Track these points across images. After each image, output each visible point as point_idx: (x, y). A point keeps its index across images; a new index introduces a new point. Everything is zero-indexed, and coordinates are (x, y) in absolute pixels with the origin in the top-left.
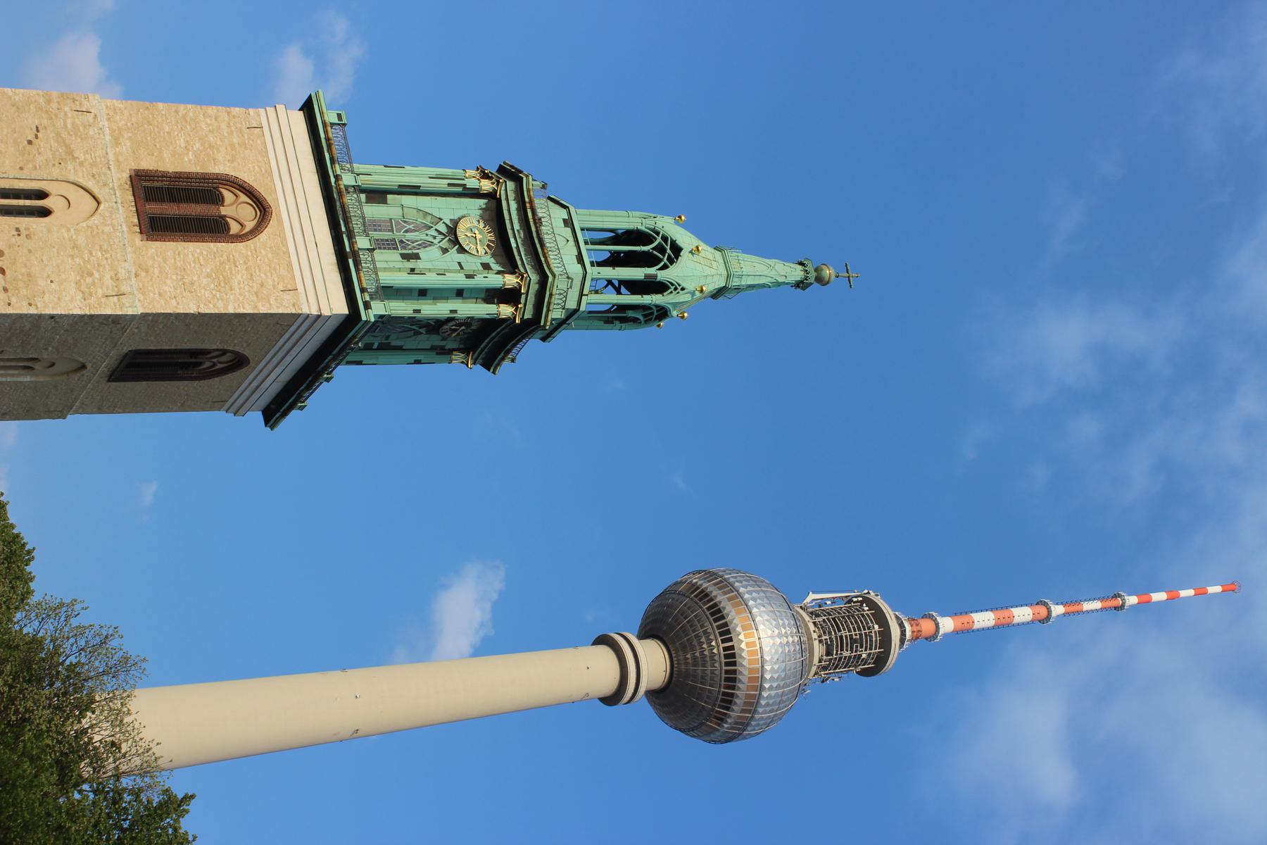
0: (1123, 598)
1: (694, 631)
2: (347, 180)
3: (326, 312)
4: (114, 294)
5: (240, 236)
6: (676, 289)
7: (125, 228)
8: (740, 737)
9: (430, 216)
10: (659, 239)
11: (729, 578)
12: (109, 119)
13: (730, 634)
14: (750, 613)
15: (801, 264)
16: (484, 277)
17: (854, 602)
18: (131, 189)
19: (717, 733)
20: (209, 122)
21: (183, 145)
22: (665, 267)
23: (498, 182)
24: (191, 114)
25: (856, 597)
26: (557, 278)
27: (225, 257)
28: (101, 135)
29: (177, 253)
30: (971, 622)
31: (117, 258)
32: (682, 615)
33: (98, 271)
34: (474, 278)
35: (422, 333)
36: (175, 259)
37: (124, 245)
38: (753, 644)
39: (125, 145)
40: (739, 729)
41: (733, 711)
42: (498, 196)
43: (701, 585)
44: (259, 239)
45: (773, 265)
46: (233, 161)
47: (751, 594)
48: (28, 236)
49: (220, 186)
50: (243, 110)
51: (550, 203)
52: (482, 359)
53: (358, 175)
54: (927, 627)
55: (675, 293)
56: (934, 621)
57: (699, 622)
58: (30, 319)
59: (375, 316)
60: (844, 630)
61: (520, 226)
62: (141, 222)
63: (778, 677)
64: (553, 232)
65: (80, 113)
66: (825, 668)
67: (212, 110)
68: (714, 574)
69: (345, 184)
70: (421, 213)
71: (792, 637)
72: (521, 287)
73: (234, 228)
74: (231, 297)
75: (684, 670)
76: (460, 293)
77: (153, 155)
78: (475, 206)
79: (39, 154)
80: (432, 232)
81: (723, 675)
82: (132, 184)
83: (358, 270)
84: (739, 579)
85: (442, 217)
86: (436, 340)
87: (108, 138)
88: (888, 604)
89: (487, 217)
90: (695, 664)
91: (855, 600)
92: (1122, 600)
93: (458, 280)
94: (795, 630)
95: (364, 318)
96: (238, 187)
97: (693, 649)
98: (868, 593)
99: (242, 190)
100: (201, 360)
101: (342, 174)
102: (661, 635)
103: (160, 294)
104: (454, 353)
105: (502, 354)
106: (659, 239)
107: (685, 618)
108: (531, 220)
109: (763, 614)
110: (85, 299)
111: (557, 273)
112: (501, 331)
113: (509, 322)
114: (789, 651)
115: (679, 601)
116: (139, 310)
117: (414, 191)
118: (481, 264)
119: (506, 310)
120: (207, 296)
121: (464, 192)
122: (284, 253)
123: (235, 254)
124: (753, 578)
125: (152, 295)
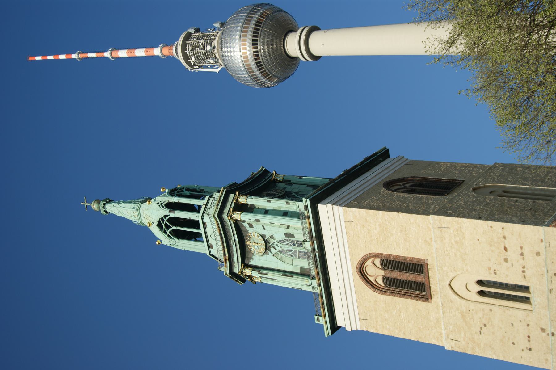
1: (271, 58)
2: (315, 282)
3: (329, 206)
4: (444, 229)
5: (374, 256)
6: (162, 204)
7: (436, 267)
8: (256, 5)
9: (279, 258)
10: (168, 232)
11: (253, 82)
12: (441, 334)
14: (243, 64)
15: (107, 212)
16: (250, 219)
17: (197, 66)
18: (431, 291)
19: (266, 8)
20: (387, 326)
22: (166, 216)
23: (242, 273)
24: (397, 331)
25: (196, 69)
26: (213, 214)
29: (409, 250)
30: (146, 52)
31: (441, 251)
32: (276, 67)
34: (256, 219)
35: (295, 193)
36: (410, 247)
37: (437, 258)
38: (243, 49)
40: (255, 9)
41: (257, 18)
42: (243, 265)
43: (266, 80)
45: (119, 213)
46: (376, 301)
47: (242, 73)
48: (490, 269)
49: (384, 288)
50: (369, 331)
51: (217, 256)
52: (267, 176)
53: (310, 285)
54: (166, 51)
55: (162, 202)
58: (493, 218)
59: (301, 201)
60: (202, 53)
61: (232, 247)
62: (427, 271)
64: (216, 241)
65: (457, 340)
66: (213, 35)
67: (385, 332)
69: (315, 281)
70: (283, 260)
71: (225, 51)
72: (233, 212)
73: (377, 262)
74: (380, 220)
75: (278, 40)
76: (267, 212)
77: (419, 310)
79: (480, 318)
80: (278, 249)
82: (431, 294)
83: (310, 229)
84: (248, 81)
85: (273, 256)
86: (289, 188)
87: (442, 323)
89: (250, 254)
90: (272, 42)
91: (197, 67)
92: (79, 56)
93: (265, 219)
94: (224, 54)
95: (308, 200)
96: (374, 286)
97: (273, 49)
98: (191, 70)
100: (410, 187)
101: (317, 286)
102: (289, 59)
103: (419, 226)
104: (281, 180)
105: (255, 177)
106: (168, 232)
107: (275, 65)
109: (237, 63)
110: (460, 227)
111: (213, 218)
112: (251, 189)
113: (245, 193)
114: (227, 44)
115: (277, 74)
116: (431, 217)
117: (286, 273)
118: (254, 228)
119: (242, 200)
120: (394, 223)
122: (351, 244)
123: (377, 246)
124: (241, 81)
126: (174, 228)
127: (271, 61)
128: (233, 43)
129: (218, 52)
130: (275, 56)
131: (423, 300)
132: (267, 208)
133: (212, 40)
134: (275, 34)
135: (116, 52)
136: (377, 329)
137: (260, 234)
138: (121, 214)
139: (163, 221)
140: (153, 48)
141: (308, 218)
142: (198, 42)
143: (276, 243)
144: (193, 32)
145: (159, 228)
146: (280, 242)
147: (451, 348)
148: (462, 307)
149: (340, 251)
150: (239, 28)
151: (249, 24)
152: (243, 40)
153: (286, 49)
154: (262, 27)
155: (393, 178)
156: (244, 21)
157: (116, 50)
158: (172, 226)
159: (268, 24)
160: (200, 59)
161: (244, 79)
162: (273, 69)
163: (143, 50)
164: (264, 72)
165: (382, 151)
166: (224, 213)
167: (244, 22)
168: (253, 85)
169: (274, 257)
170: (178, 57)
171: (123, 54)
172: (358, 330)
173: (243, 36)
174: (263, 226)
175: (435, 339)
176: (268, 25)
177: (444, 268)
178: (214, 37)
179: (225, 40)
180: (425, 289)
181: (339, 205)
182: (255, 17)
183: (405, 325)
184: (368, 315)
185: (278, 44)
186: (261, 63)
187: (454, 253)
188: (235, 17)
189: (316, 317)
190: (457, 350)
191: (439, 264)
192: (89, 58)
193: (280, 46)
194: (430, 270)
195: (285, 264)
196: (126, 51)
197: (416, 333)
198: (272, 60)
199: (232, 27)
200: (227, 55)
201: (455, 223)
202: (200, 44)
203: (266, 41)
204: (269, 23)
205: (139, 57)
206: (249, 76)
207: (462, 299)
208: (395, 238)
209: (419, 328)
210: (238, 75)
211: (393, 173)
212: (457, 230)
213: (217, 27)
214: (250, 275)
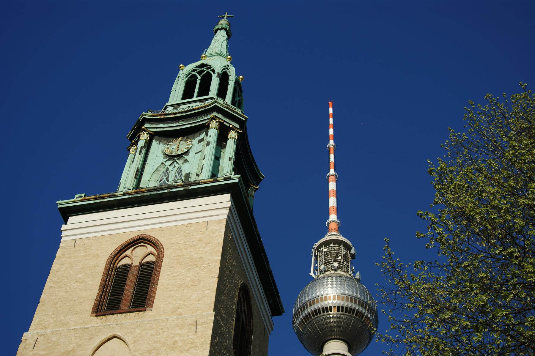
0: (330, 145)
1: (323, 325)
3: (229, 204)
4: (195, 328)
6: (227, 69)
10: (195, 73)
11: (300, 305)
12: (46, 328)
13: (328, 307)
15: (216, 31)
17: (318, 254)
21: (79, 284)
22: (213, 71)
25: (315, 253)
27: (175, 261)
28: (58, 332)
30: (334, 207)
33: (174, 337)
36: (171, 291)
37: (154, 320)
39: (70, 319)
41: (365, 313)
43: (301, 319)
44: (163, 242)
47: (310, 295)
49: (116, 265)
54: (333, 226)
56: (331, 222)
57: (320, 322)
63: (352, 292)
66: (348, 272)
67: (55, 266)
68: (296, 312)
71: (333, 279)
72: (219, 122)
73: (151, 258)
74: (208, 258)
78: (157, 148)
80: (171, 168)
81: (347, 314)
82: (103, 315)
83: (199, 183)
84: (301, 301)
85: (161, 162)
88: (319, 240)
89: (165, 142)
90: (340, 327)
95: (237, 181)
96: (119, 254)
98: (314, 248)
99: (122, 252)
103: (199, 300)
106: (195, 73)
107: (316, 328)
108: (173, 116)
109: (320, 291)
114: (340, 281)
119: (232, 135)
121: (146, 148)
125: (199, 305)
126: (199, 78)
127: (320, 324)
128: (340, 287)
129: (331, 274)
130: (325, 329)
131: (95, 307)
132: (221, 160)
133: (343, 269)
134: (348, 330)
135: (335, 179)
136: (60, 257)
137: (190, 150)
138: (214, 42)
139: (208, 69)
140: (337, 214)
141: (213, 181)
142: (342, 256)
143: (177, 166)
144: (351, 252)
145: (199, 65)
146: (179, 169)
147: (25, 339)
148: (82, 350)
149: (147, 220)
150: (355, 294)
151: (359, 305)
152: (343, 297)
153: (332, 341)
154: (355, 318)
155: (252, 302)
156: (362, 300)
157: (336, 180)
158: (201, 76)
159: (358, 324)
160: (325, 257)
161: (304, 297)
162: (312, 326)
163: (335, 205)
164: (309, 316)
165: (280, 304)
166: (218, 114)
167: (361, 300)
168: (296, 306)
169: (161, 164)
170: (328, 236)
171: (332, 186)
172: (61, 238)
173: (347, 298)
174: (201, 151)
175: (40, 321)
176: (357, 323)
177: (139, 329)
178: (346, 271)
179: (344, 280)
180: (110, 310)
181: (229, 215)
182: (365, 311)
183: (63, 288)
184: (81, 248)
185: (338, 332)
186: (319, 314)
187: (160, 341)
188: (366, 291)
189: (83, 195)
190: (21, 346)
191: (145, 322)
192: (329, 155)
193: (335, 334)
194: (137, 314)
195: (152, 174)
196: (335, 189)
197: (51, 300)
198: (321, 326)
199: (357, 288)
200: (329, 280)
201: (203, 340)
202: (340, 258)
203: (341, 320)
204: (359, 325)
205: (328, 200)
206: (306, 301)
207: (93, 351)
208: (183, 275)
209: (57, 303)
210: (308, 290)
211: (257, 306)
212: (193, 343)
213: (356, 275)
214: (140, 139)
